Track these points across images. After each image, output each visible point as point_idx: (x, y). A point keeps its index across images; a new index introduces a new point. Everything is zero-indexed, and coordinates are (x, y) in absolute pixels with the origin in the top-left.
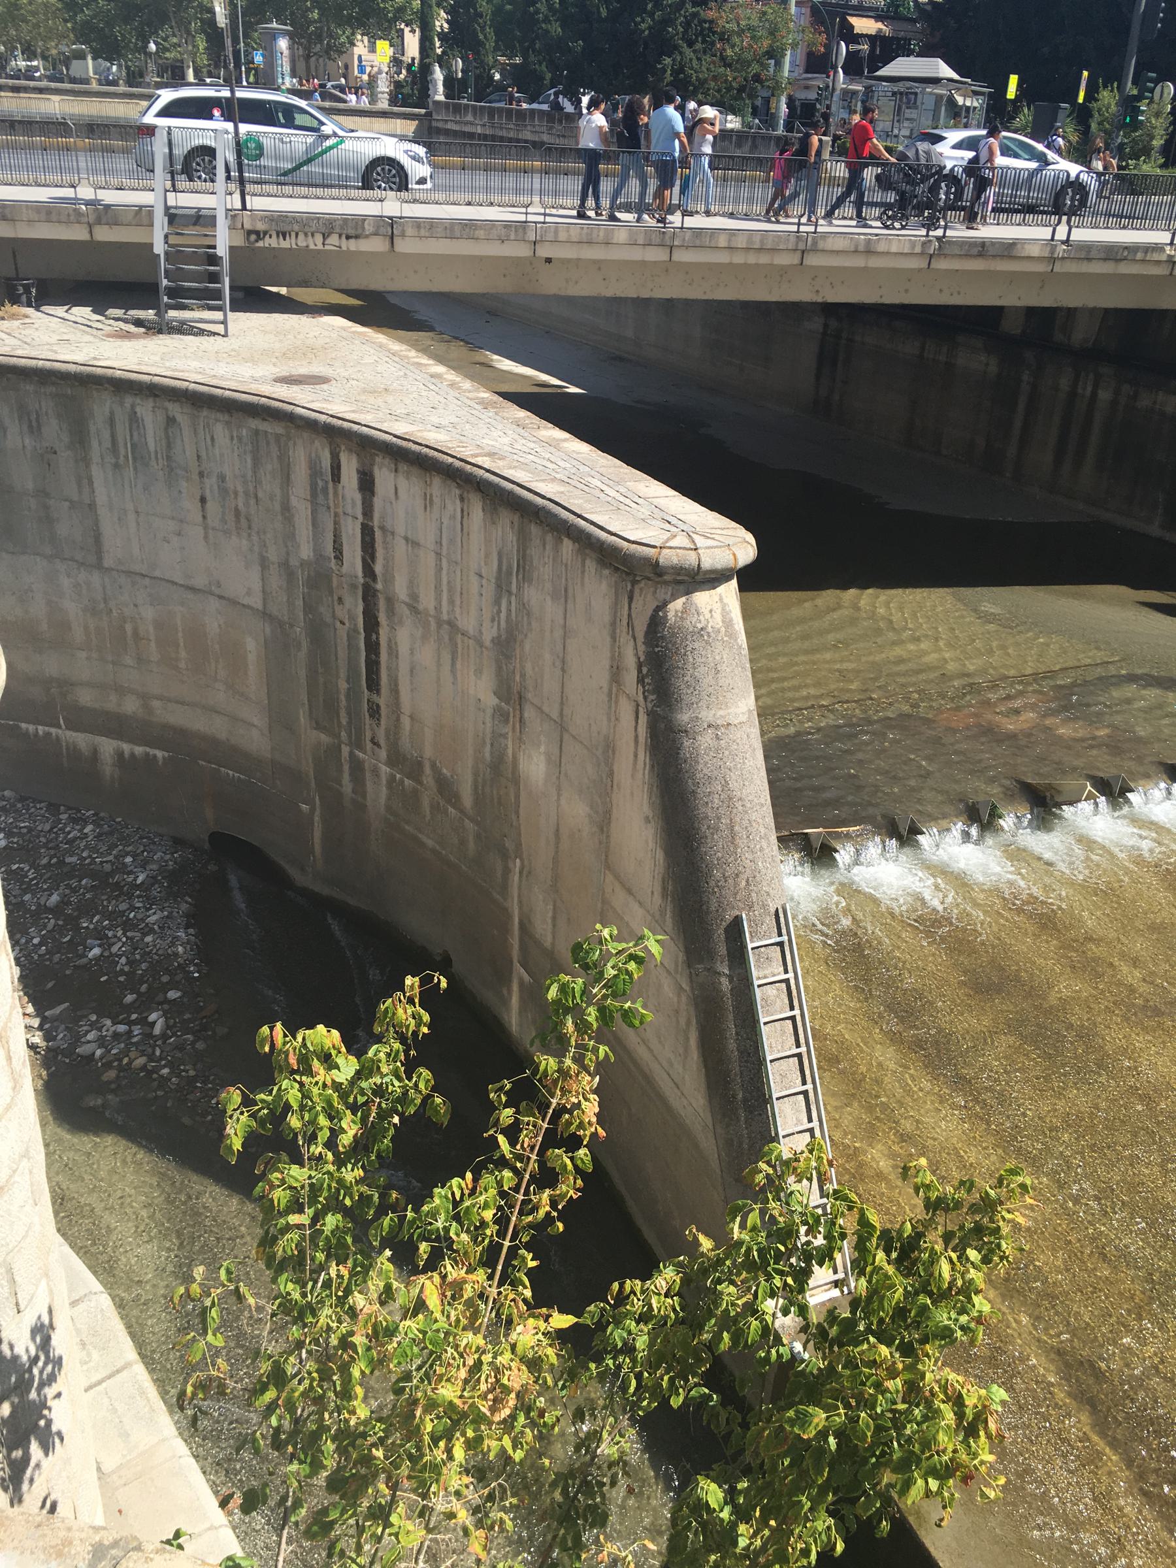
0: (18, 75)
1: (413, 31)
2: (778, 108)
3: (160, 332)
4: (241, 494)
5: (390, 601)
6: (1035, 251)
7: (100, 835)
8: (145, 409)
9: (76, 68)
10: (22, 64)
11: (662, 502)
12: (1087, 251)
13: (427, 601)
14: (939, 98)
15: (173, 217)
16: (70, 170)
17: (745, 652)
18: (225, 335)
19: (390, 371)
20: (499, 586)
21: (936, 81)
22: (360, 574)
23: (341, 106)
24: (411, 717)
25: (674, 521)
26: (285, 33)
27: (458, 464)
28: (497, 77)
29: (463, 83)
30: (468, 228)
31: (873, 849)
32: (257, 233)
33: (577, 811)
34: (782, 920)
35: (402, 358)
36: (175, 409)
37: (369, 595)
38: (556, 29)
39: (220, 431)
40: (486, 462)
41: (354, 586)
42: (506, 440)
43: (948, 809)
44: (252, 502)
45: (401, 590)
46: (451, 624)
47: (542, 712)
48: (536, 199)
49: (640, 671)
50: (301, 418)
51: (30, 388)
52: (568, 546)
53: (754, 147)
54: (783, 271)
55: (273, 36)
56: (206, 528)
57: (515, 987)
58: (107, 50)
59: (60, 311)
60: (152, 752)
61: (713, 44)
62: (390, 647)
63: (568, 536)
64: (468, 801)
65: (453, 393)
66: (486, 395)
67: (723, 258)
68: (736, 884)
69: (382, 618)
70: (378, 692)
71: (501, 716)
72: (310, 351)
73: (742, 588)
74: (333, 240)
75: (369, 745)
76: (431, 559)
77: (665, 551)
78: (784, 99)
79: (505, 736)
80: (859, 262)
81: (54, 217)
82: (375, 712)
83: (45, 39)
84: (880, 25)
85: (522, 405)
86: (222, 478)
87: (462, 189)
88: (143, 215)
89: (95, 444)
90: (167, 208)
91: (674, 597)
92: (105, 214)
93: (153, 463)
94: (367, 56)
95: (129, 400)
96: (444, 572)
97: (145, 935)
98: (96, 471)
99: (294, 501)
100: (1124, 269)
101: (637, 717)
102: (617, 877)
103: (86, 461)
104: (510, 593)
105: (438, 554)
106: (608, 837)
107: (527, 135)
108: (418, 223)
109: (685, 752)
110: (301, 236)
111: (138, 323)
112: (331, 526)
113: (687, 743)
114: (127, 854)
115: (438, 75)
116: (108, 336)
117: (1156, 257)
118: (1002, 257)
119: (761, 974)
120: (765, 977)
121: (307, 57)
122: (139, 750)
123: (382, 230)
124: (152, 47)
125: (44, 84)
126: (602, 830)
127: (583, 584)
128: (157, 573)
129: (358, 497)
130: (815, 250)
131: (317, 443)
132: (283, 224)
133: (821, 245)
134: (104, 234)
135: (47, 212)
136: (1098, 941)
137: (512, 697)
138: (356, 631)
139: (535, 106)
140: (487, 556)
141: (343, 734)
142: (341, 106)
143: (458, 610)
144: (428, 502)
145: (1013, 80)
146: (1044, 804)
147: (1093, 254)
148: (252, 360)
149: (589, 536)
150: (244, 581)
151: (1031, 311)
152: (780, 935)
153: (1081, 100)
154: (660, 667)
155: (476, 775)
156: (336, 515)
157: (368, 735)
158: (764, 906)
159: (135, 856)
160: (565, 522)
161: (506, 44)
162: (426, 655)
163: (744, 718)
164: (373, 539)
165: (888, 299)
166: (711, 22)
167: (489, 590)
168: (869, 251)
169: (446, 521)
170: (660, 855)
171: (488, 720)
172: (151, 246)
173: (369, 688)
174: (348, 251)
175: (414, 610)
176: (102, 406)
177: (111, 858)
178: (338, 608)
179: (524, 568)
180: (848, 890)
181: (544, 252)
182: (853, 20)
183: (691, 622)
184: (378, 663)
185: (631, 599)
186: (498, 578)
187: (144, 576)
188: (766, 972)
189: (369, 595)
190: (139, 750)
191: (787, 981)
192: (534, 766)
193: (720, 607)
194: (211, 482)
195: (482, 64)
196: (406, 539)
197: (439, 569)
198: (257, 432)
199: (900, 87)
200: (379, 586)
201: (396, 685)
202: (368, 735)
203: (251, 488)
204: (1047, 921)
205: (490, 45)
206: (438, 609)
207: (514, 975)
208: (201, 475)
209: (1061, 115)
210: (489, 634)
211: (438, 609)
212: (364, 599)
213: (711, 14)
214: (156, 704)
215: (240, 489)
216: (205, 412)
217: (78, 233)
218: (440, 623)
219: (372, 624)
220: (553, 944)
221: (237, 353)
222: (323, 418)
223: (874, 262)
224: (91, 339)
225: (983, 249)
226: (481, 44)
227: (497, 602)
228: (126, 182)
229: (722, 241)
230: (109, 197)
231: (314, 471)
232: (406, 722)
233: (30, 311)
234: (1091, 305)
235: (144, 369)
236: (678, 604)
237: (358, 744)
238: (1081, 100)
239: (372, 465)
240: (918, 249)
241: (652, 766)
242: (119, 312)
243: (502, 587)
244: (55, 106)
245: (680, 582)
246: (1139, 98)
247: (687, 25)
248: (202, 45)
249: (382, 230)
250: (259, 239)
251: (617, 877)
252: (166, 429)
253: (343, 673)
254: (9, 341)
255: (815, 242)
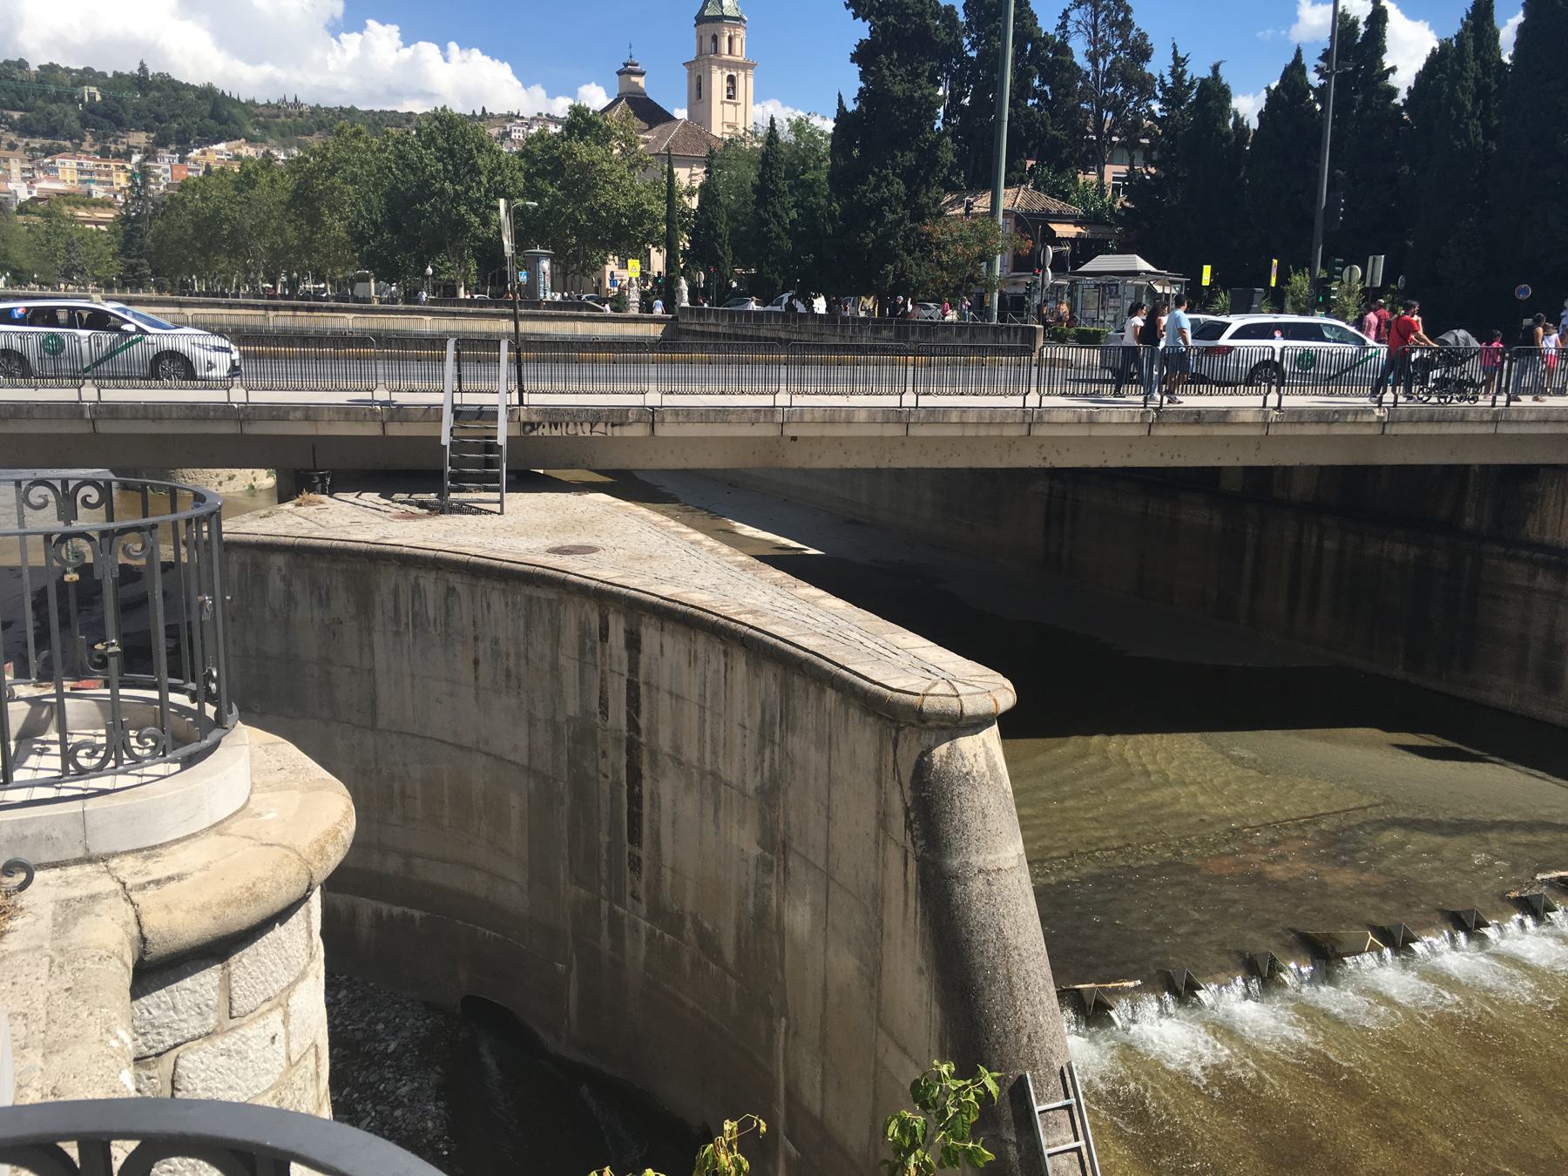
0: (306, 296)
1: (659, 251)
2: (991, 302)
3: (442, 512)
4: (512, 656)
5: (654, 754)
6: (1249, 417)
7: (353, 1001)
8: (428, 582)
9: (360, 289)
10: (310, 286)
11: (919, 652)
12: (1298, 416)
13: (691, 753)
14: (1139, 288)
15: (459, 413)
16: (369, 377)
17: (1011, 796)
18: (501, 513)
19: (653, 540)
20: (762, 736)
21: (1136, 274)
22: (625, 728)
23: (597, 314)
24: (673, 870)
25: (933, 670)
26: (548, 256)
27: (723, 621)
28: (735, 285)
29: (705, 293)
30: (722, 414)
31: (1150, 1006)
32: (532, 424)
33: (845, 964)
34: (1068, 1080)
35: (663, 528)
36: (455, 580)
37: (633, 748)
38: (788, 244)
39: (496, 599)
40: (749, 619)
41: (618, 740)
42: (766, 599)
43: (1224, 960)
44: (523, 662)
45: (664, 742)
46: (714, 774)
47: (807, 860)
48: (783, 387)
49: (907, 816)
50: (573, 584)
51: (324, 565)
52: (831, 696)
53: (973, 336)
54: (1011, 442)
55: (537, 259)
56: (477, 689)
57: (782, 1165)
58: (387, 273)
59: (351, 497)
60: (410, 911)
61: (931, 252)
62: (652, 799)
63: (832, 686)
64: (730, 955)
65: (713, 558)
66: (743, 558)
67: (955, 432)
68: (1018, 1041)
69: (645, 770)
70: (640, 846)
71: (765, 865)
72: (578, 525)
73: (1004, 735)
74: (600, 427)
75: (629, 899)
76: (695, 712)
77: (928, 698)
78: (996, 295)
79: (769, 886)
80: (1083, 432)
81: (352, 416)
82: (636, 864)
83: (333, 266)
84: (1079, 229)
85: (778, 567)
86: (496, 641)
87: (717, 380)
88: (433, 413)
89: (378, 614)
90: (454, 406)
91: (939, 743)
92: (399, 413)
93: (432, 629)
94: (618, 272)
95: (413, 573)
96: (708, 724)
97: (394, 1108)
98: (377, 638)
99: (563, 661)
100: (1337, 430)
101: (906, 864)
102: (890, 1034)
103: (369, 630)
104: (772, 742)
105: (702, 708)
106: (879, 991)
107: (763, 332)
108: (676, 411)
109: (957, 899)
110: (571, 426)
111: (422, 505)
112: (597, 683)
113: (958, 889)
114: (379, 1020)
115: (684, 285)
116: (396, 517)
117: (1366, 418)
118: (1218, 423)
119: (1051, 1142)
120: (1055, 1145)
121: (565, 275)
122: (397, 910)
123: (644, 418)
124: (430, 270)
125: (332, 304)
126: (873, 985)
127: (846, 730)
128: (428, 734)
129: (624, 655)
130: (1040, 422)
131: (587, 607)
132: (554, 416)
133: (1046, 418)
134: (395, 430)
135: (345, 412)
136: (1402, 1107)
137: (776, 846)
138: (618, 783)
139: (769, 308)
140: (750, 708)
141: (603, 888)
142: (597, 314)
143: (720, 760)
144: (693, 658)
145: (1207, 269)
146: (1326, 956)
147: (1305, 418)
148: (525, 533)
149: (853, 685)
150: (511, 738)
151: (1248, 470)
152: (1067, 1097)
153: (1273, 284)
154: (929, 811)
155: (739, 928)
156: (603, 672)
157: (629, 889)
158: (1048, 1064)
159: (387, 1022)
160: (829, 673)
161: (743, 259)
162: (689, 806)
163: (1014, 863)
164: (638, 695)
165: (1112, 464)
166: (929, 235)
167: (753, 740)
168: (1091, 422)
169: (710, 674)
170: (936, 1010)
171: (752, 870)
172: (439, 438)
173: (631, 841)
174: (613, 437)
175: (678, 762)
176: (387, 580)
177: (362, 1025)
178: (602, 762)
179: (787, 719)
180: (1128, 1051)
181: (790, 431)
182: (1054, 227)
183: (957, 766)
184: (640, 815)
185: (896, 745)
186: (762, 728)
187: (414, 735)
188: (1057, 1139)
189: (633, 748)
190: (397, 910)
191: (1078, 1150)
192: (799, 918)
193: (983, 752)
194: (484, 646)
195: (721, 275)
196: (671, 693)
197: (703, 721)
198: (530, 599)
199: (1103, 280)
200: (643, 739)
201: (658, 837)
202: (629, 889)
203: (522, 648)
204: (1348, 1087)
205: (729, 259)
206: (701, 760)
207: (781, 1149)
208: (476, 638)
209: (1257, 298)
210: (752, 784)
211: (701, 760)
212: (628, 752)
213: (927, 229)
214: (418, 862)
215: (512, 650)
216: (483, 582)
217: (372, 430)
218: (703, 774)
219: (635, 776)
220: (822, 1111)
221: (516, 529)
222: (594, 583)
223: (1097, 432)
224: (379, 520)
225: (1198, 416)
226: (721, 259)
227: (760, 751)
228: (416, 385)
229: (954, 418)
230: (402, 398)
231: (584, 632)
232: (667, 874)
233: (324, 497)
234: (1308, 462)
235: (429, 545)
236: (942, 750)
237: (619, 900)
238: (1273, 284)
239: (639, 625)
240: (1138, 419)
241: (924, 914)
242: (404, 496)
243: (765, 737)
244: (349, 322)
245: (943, 728)
246: (1330, 280)
247: (906, 238)
248: (473, 267)
249: (644, 418)
250: (533, 429)
251: (890, 1034)
252: (446, 599)
253: (604, 827)
254: (307, 524)
255: (1040, 416)
